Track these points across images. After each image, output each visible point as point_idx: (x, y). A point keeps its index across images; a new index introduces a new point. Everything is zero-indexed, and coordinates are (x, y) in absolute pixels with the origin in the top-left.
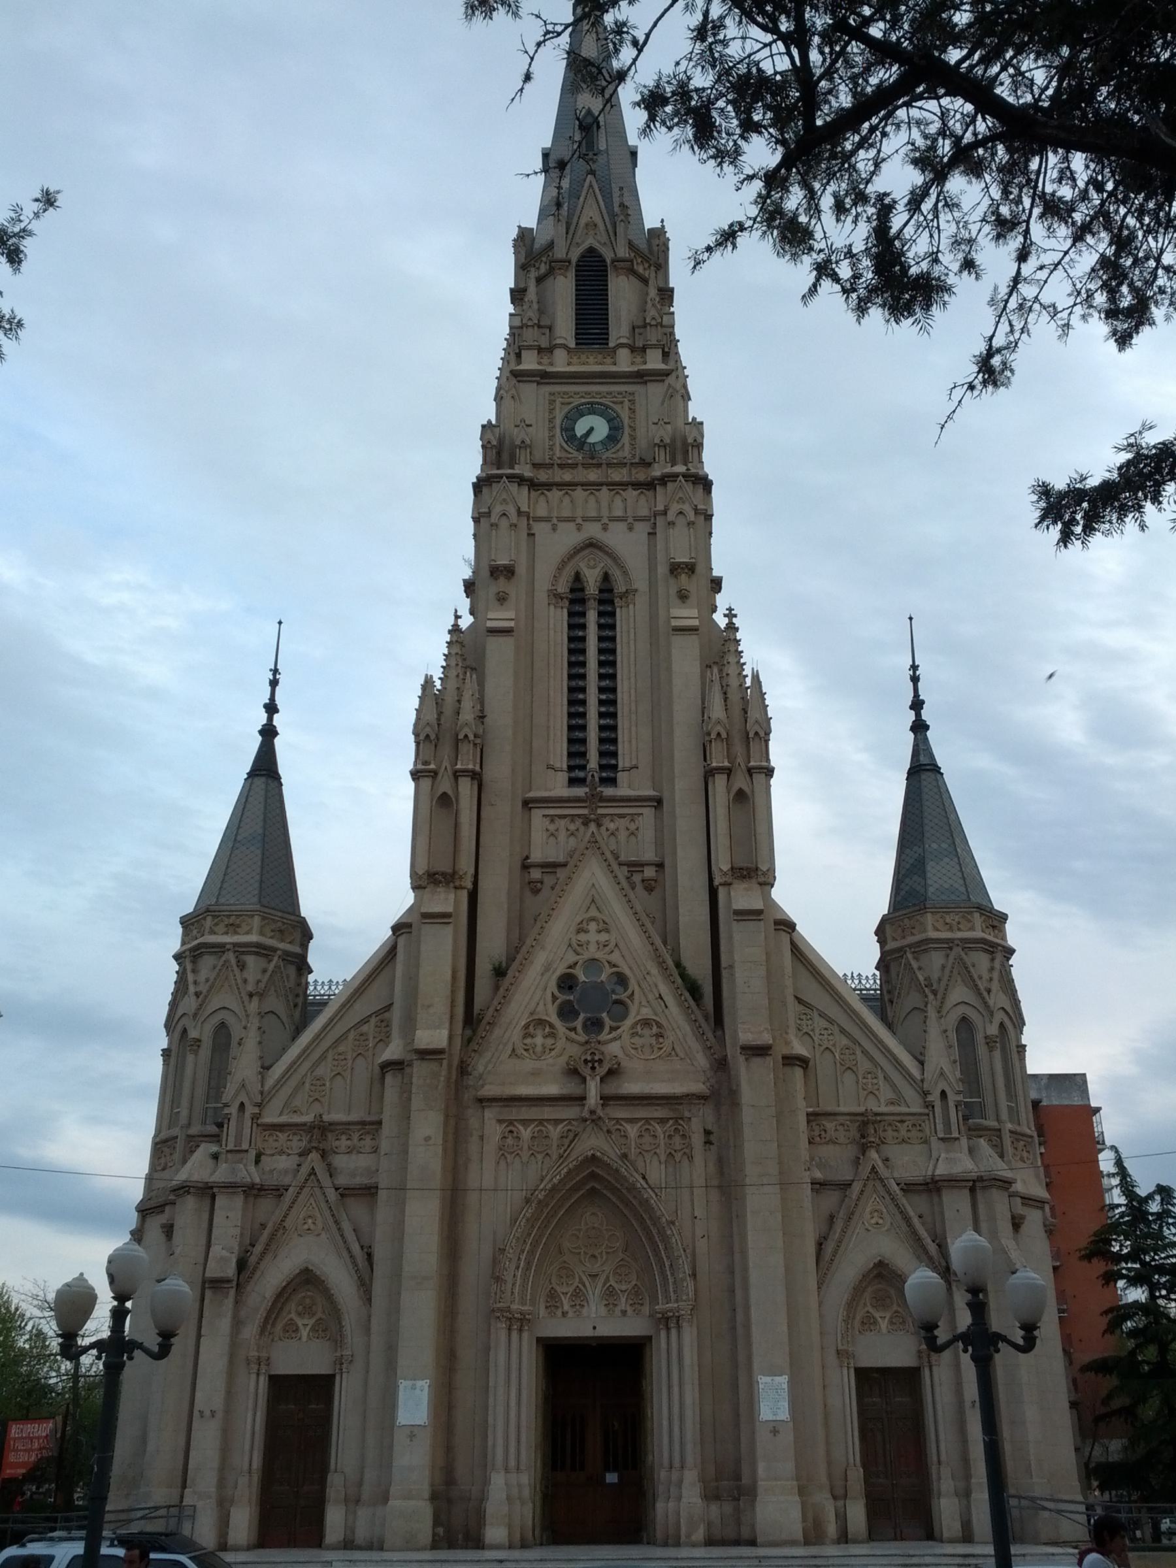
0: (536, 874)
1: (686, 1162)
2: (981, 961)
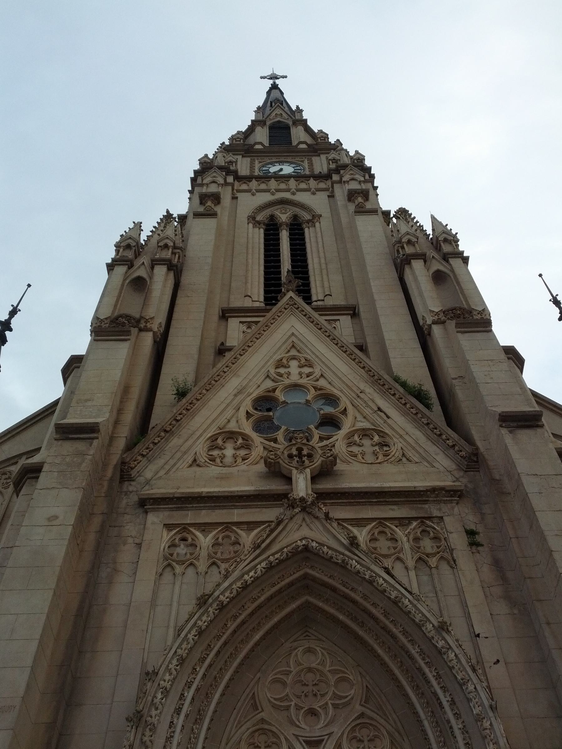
1: (444, 566)
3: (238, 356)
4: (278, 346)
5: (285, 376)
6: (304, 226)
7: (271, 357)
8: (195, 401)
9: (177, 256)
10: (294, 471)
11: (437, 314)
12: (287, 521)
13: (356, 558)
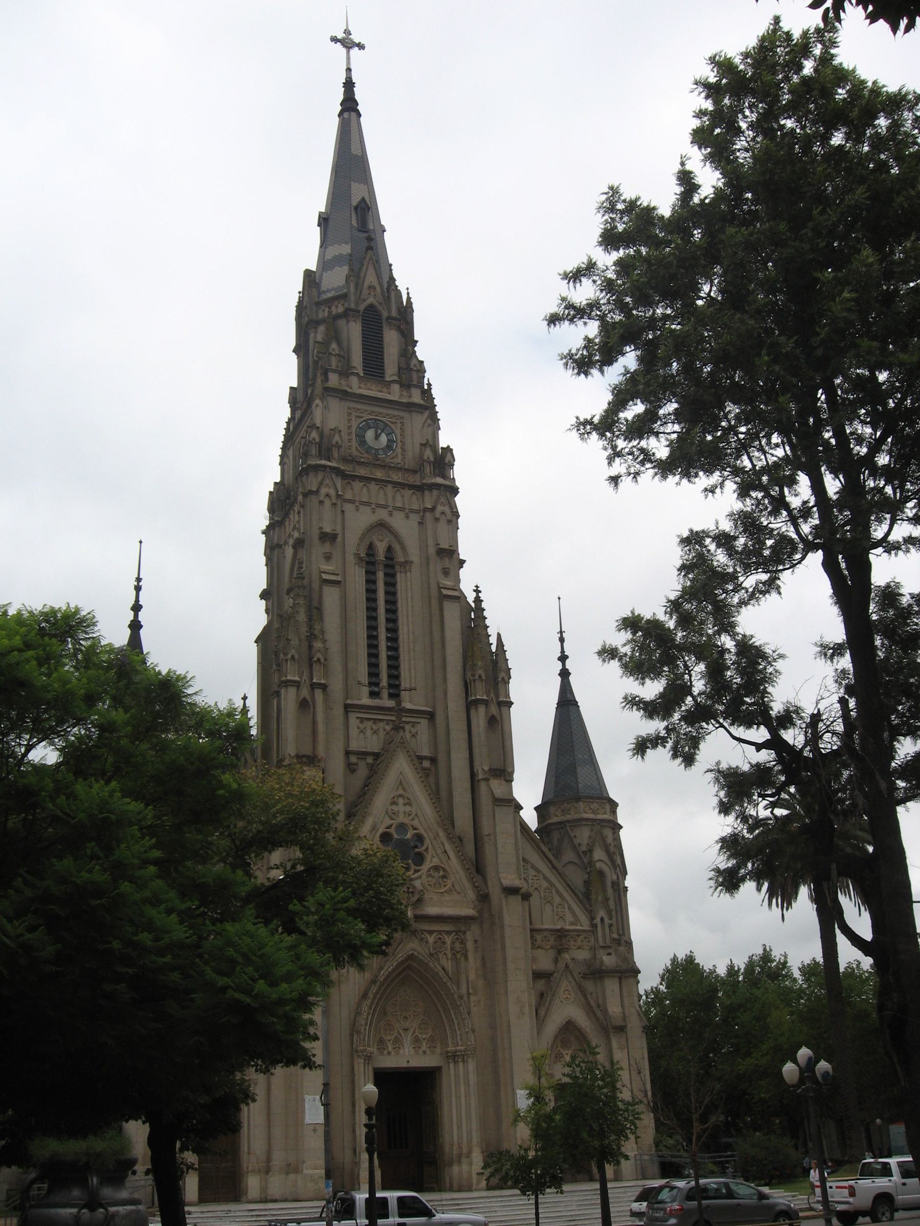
0: (353, 759)
1: (463, 959)
2: (608, 832)
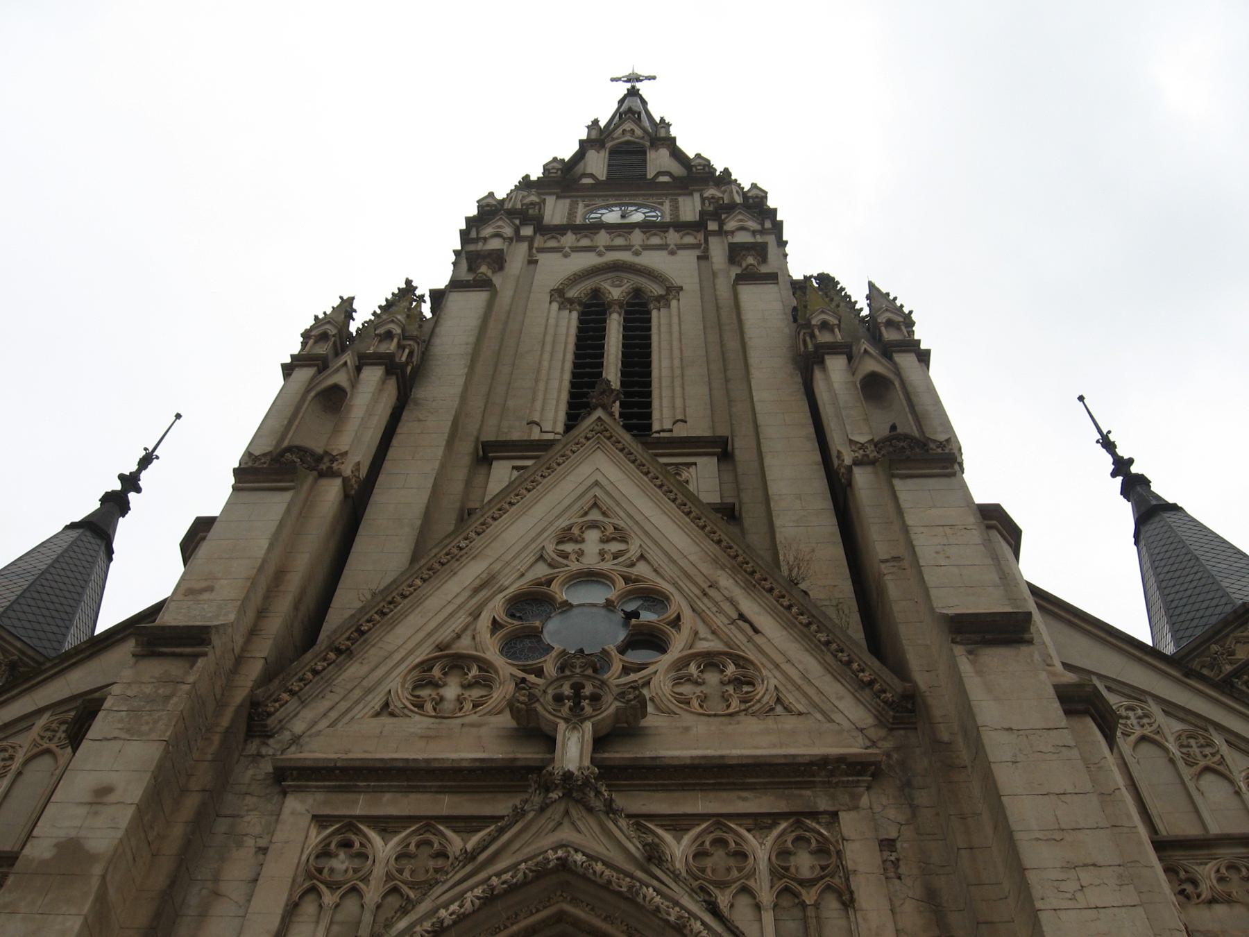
1: (832, 905)
3: (490, 520)
4: (567, 502)
5: (573, 557)
6: (652, 306)
7: (551, 523)
8: (398, 599)
9: (407, 351)
10: (562, 725)
11: (863, 446)
12: (531, 815)
13: (655, 883)
